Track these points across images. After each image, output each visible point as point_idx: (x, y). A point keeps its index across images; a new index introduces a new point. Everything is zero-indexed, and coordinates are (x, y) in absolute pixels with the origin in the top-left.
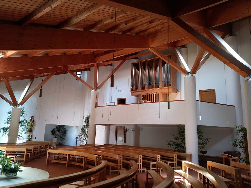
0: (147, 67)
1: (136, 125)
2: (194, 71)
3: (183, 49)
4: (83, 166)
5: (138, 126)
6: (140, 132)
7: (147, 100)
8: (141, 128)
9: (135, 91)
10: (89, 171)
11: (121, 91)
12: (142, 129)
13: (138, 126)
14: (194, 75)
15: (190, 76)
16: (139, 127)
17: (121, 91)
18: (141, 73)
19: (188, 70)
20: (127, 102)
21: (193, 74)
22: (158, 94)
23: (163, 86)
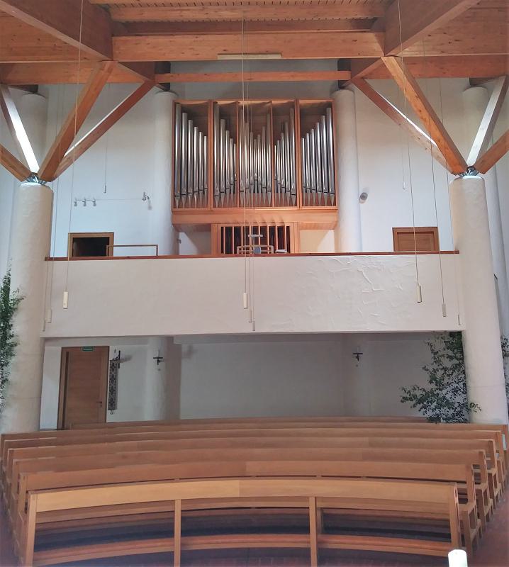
0: (243, 129)
1: (169, 339)
2: (50, 172)
3: (30, 98)
4: (309, 550)
5: (176, 342)
6: (183, 362)
7: (273, 243)
8: (185, 348)
9: (190, 209)
10: (401, 550)
11: (90, 204)
12: (190, 352)
13: (176, 342)
14: (48, 184)
15: (36, 183)
16: (179, 347)
17: (90, 204)
18: (196, 144)
19: (34, 166)
20: (117, 252)
21: (46, 181)
22: (288, 228)
23: (306, 203)
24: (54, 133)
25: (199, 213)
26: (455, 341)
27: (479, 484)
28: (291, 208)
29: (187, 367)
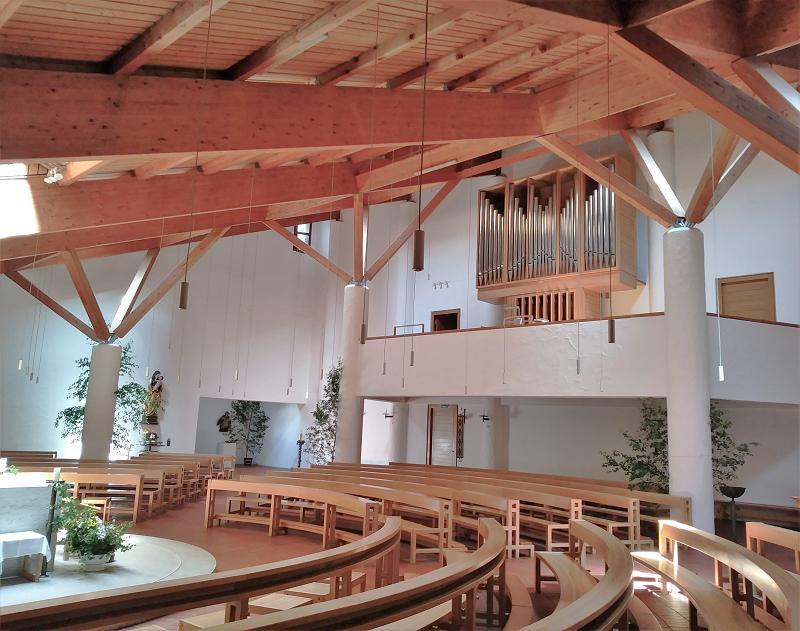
0: (532, 201)
1: (497, 400)
3: (658, 137)
5: (503, 403)
6: (511, 421)
8: (512, 409)
11: (444, 286)
12: (516, 413)
13: (503, 403)
14: (696, 226)
15: (684, 228)
17: (444, 286)
19: (677, 206)
22: (572, 295)
24: (696, 170)
25: (493, 288)
26: (653, 415)
27: (437, 520)
28: (571, 275)
29: (515, 427)
